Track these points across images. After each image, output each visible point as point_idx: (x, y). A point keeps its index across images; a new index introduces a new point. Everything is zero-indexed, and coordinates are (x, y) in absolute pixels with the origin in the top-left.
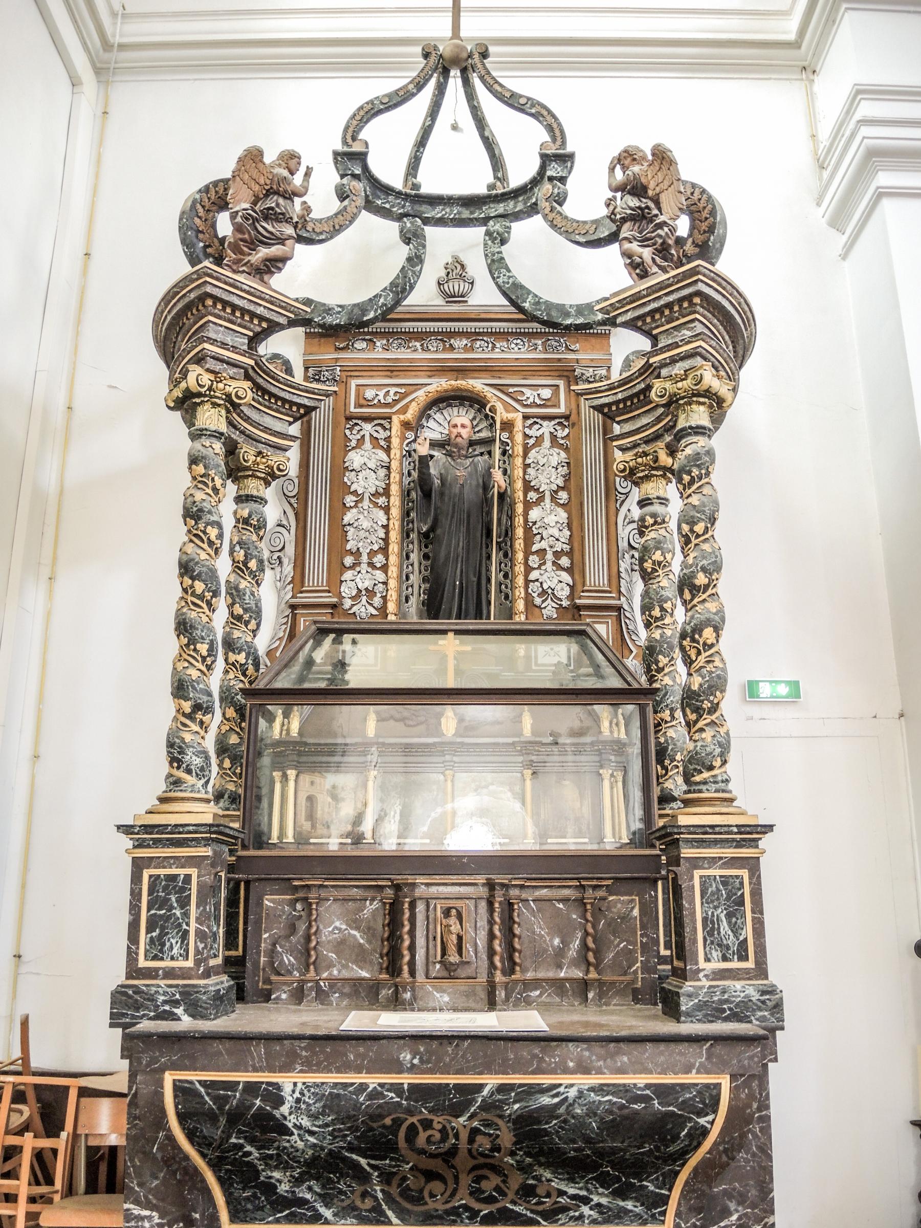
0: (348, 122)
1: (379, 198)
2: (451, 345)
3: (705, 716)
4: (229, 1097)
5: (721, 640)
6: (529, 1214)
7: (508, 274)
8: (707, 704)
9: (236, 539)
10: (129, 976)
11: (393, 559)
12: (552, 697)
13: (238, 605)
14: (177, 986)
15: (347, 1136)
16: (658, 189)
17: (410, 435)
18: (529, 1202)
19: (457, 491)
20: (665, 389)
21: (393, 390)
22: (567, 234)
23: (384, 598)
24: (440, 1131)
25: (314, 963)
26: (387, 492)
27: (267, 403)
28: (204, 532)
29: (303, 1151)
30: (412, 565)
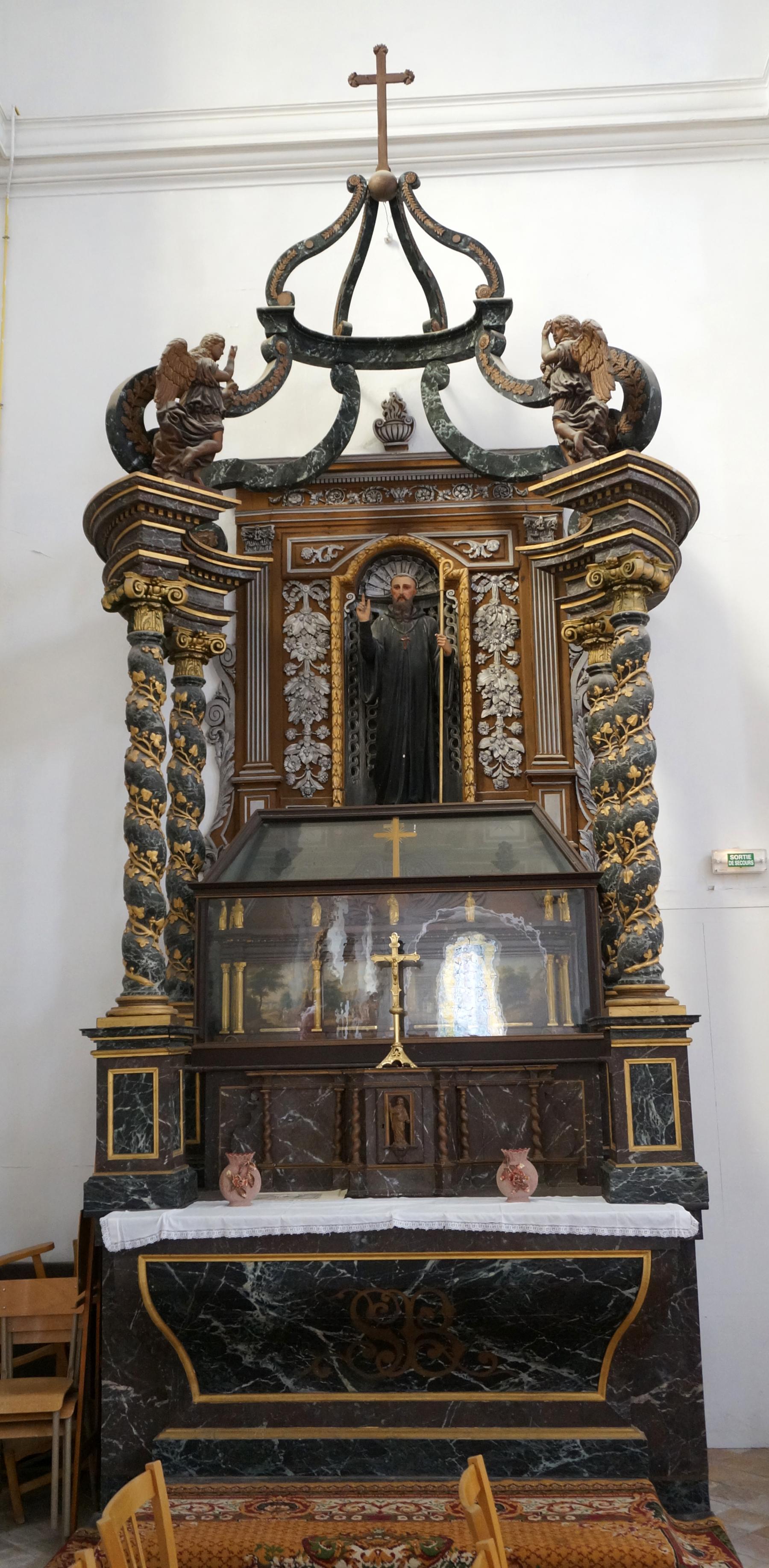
0: (272, 272)
1: (308, 348)
2: (391, 495)
3: (637, 909)
4: (196, 1276)
5: (655, 832)
6: (472, 1380)
7: (447, 424)
8: (638, 897)
9: (176, 724)
10: (99, 1168)
11: (337, 732)
14: (144, 1177)
15: (303, 1309)
16: (589, 366)
17: (351, 597)
18: (471, 1369)
19: (401, 658)
20: (599, 575)
21: (331, 548)
22: (506, 393)
23: (329, 772)
24: (388, 1304)
25: (270, 1151)
26: (328, 659)
27: (201, 580)
28: (149, 739)
29: (265, 1325)
30: (358, 734)
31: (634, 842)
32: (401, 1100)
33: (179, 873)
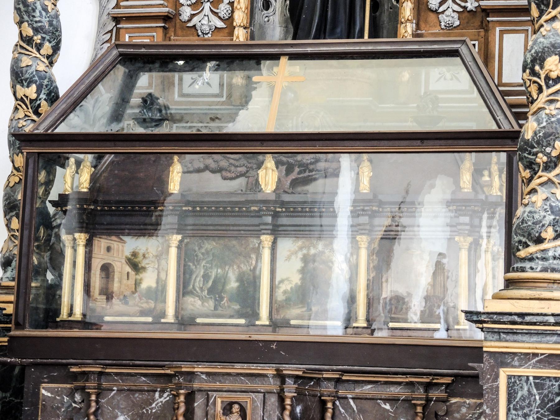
3: (540, 173)
8: (541, 159)
12: (391, 143)
13: (26, 24)
31: (543, 84)
32: (236, 408)
33: (22, 123)
